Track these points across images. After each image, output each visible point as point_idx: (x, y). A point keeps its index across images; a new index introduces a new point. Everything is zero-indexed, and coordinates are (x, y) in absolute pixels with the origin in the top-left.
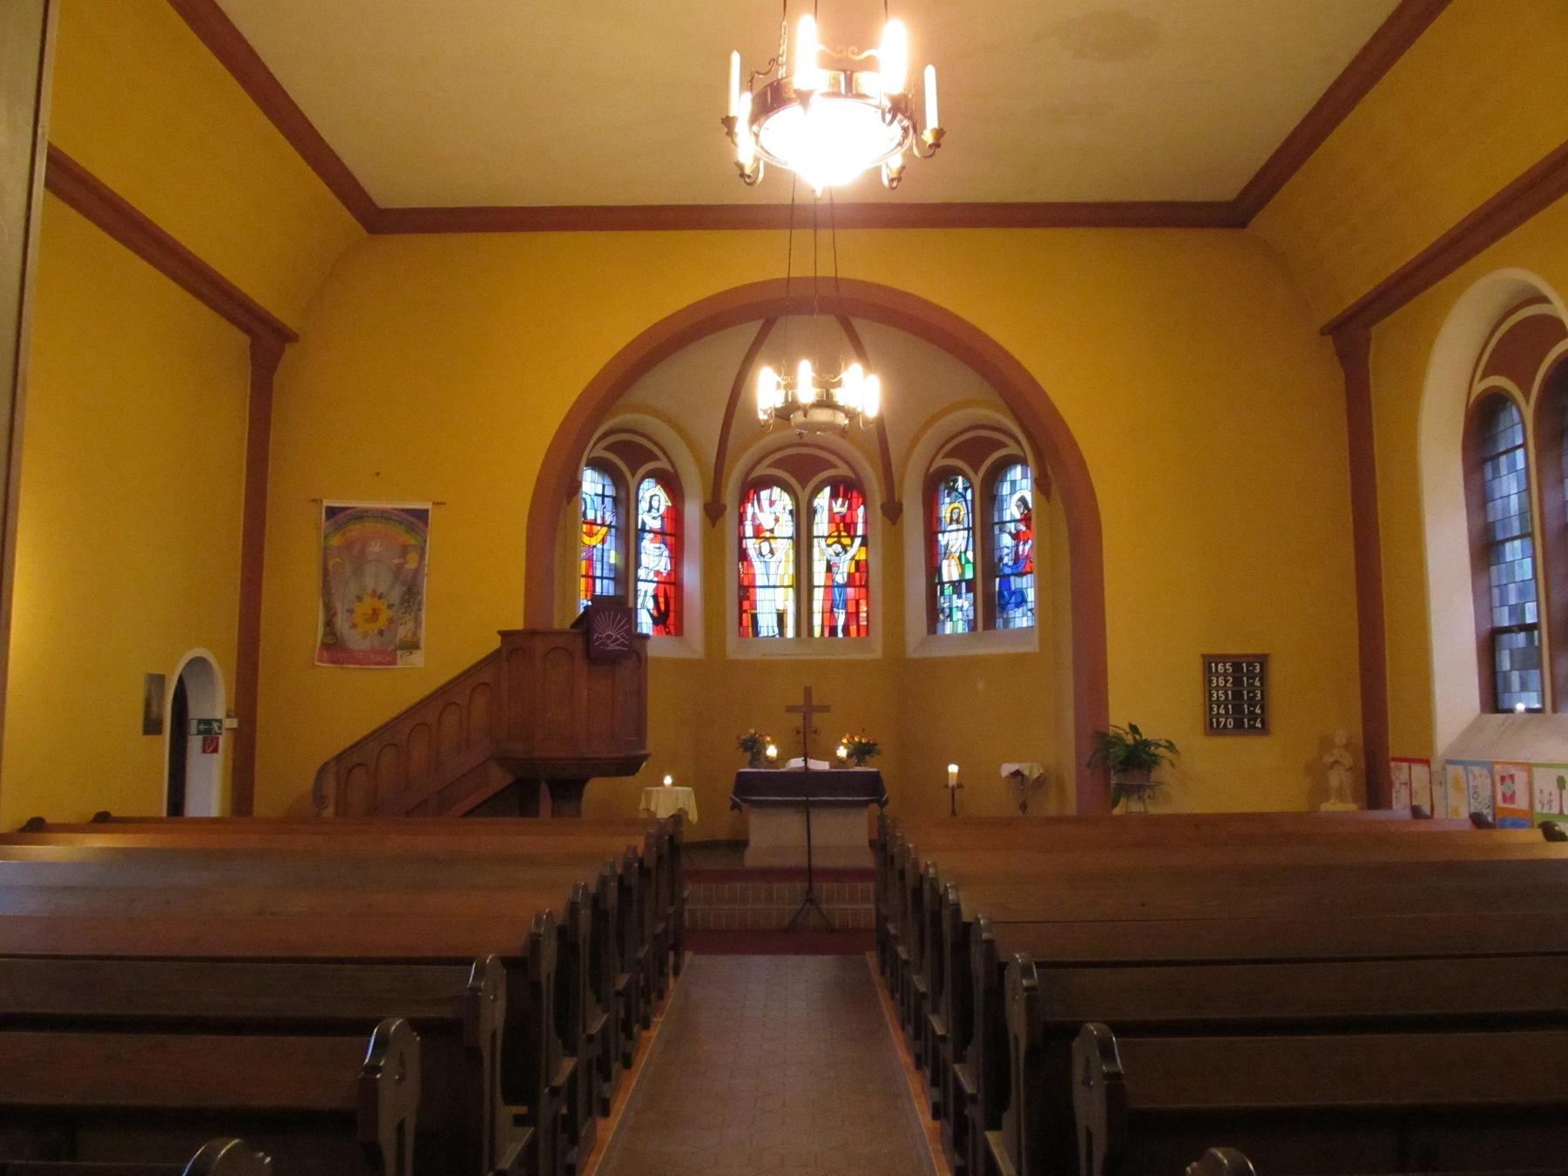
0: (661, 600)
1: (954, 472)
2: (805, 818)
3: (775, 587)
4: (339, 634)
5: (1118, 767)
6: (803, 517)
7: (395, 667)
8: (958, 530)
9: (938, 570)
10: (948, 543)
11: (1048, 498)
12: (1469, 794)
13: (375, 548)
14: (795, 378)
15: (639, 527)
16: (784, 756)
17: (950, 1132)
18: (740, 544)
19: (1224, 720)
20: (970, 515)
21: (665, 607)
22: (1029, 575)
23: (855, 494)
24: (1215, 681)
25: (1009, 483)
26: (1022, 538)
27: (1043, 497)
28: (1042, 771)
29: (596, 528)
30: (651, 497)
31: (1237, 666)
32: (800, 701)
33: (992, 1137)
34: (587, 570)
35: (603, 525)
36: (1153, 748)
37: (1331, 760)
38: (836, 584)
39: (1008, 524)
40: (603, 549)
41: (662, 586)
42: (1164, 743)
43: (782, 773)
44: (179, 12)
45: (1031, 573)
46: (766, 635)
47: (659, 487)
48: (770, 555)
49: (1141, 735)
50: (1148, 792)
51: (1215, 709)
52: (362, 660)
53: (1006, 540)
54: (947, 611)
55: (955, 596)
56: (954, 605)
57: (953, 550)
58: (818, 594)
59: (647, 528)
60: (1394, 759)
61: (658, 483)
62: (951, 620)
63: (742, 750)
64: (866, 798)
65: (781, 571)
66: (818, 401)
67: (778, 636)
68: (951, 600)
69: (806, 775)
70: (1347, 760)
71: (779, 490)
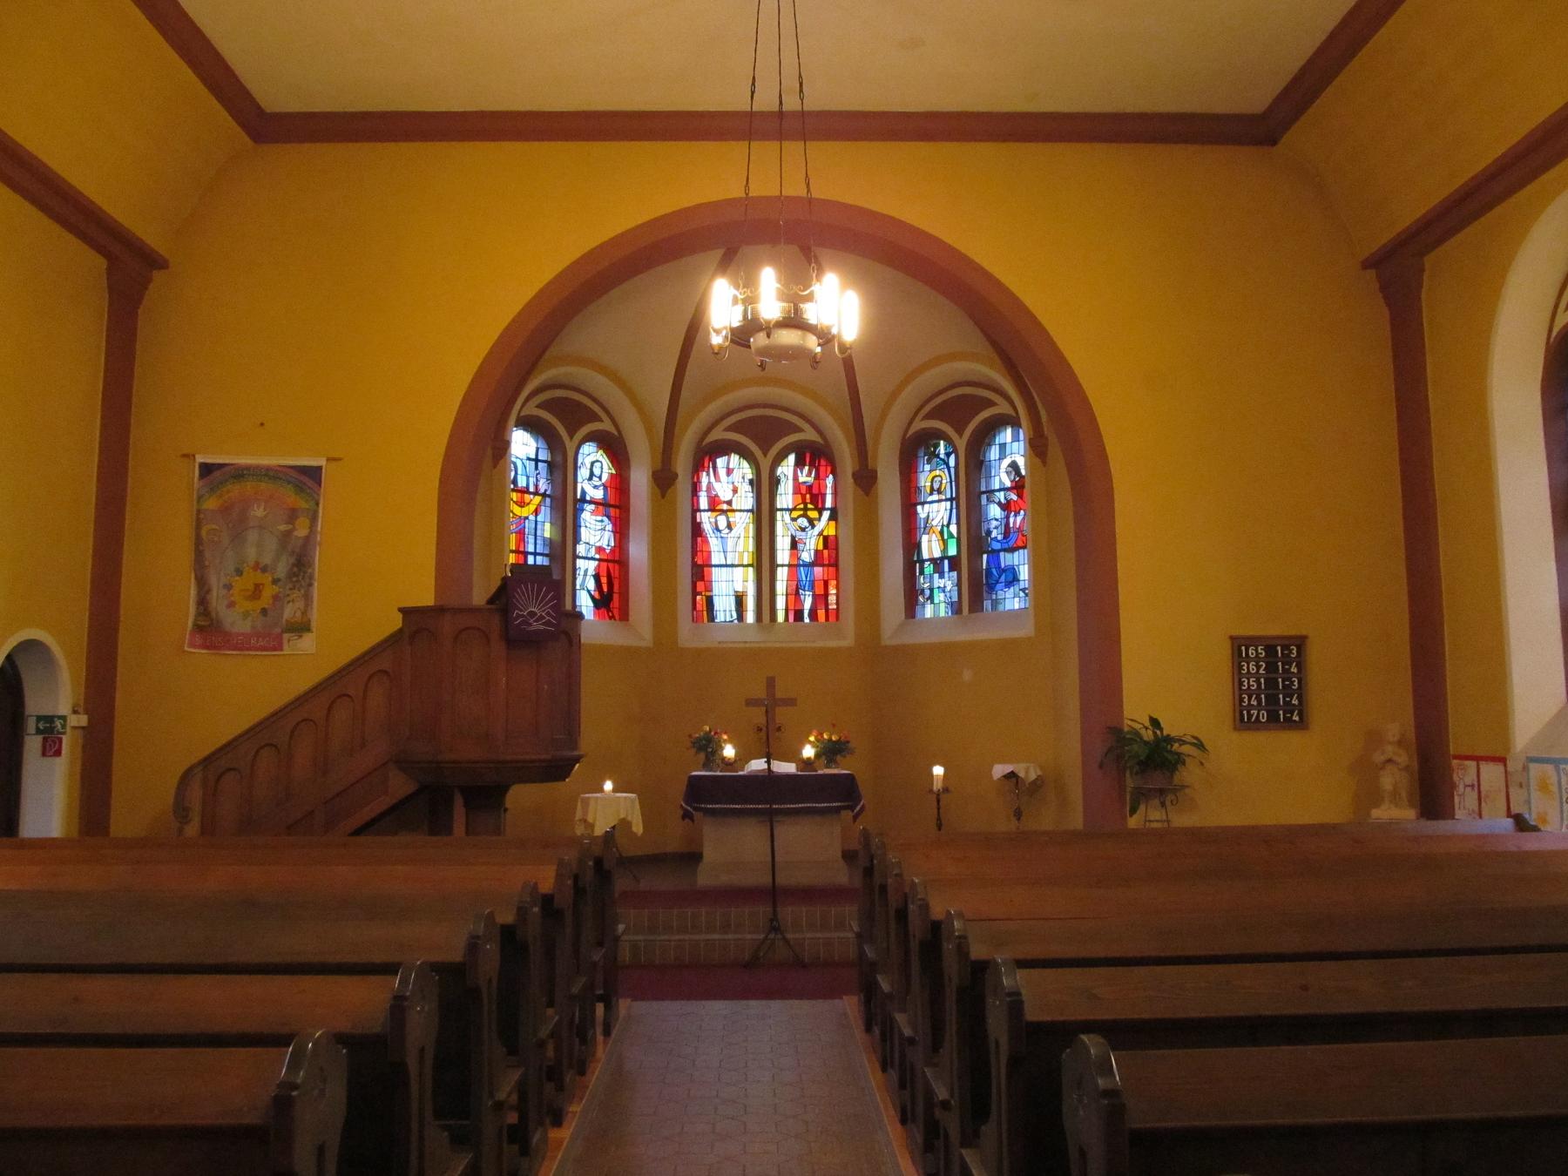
0: (604, 580)
1: (939, 435)
2: (769, 828)
3: (732, 566)
4: (214, 615)
5: (1137, 768)
6: (765, 487)
7: (282, 653)
8: (939, 501)
9: (918, 546)
10: (928, 516)
11: (1044, 463)
12: (1561, 798)
13: (258, 512)
14: (756, 289)
15: (579, 497)
16: (743, 758)
17: (919, 1139)
18: (694, 518)
19: (1256, 712)
20: (953, 483)
22: (1022, 551)
23: (823, 462)
24: (1245, 668)
25: (997, 447)
26: (1013, 509)
27: (1037, 460)
28: (1039, 773)
29: (527, 497)
31: (1270, 649)
33: (969, 1156)
34: (518, 545)
35: (536, 493)
36: (1176, 745)
37: (1383, 758)
39: (997, 494)
40: (536, 521)
42: (1188, 739)
43: (740, 776)
44: (159, 32)
45: (1024, 547)
46: (723, 620)
47: (601, 452)
48: (727, 531)
49: (1161, 730)
50: (1170, 797)
51: (1246, 700)
52: (241, 644)
53: (995, 511)
54: (927, 592)
55: (936, 576)
56: (936, 585)
57: (934, 523)
58: (782, 574)
59: (588, 498)
60: (1456, 757)
62: (932, 602)
63: (694, 750)
64: (839, 804)
65: (740, 548)
66: (784, 318)
67: (736, 621)
69: (769, 778)
70: (1403, 758)
71: (737, 457)
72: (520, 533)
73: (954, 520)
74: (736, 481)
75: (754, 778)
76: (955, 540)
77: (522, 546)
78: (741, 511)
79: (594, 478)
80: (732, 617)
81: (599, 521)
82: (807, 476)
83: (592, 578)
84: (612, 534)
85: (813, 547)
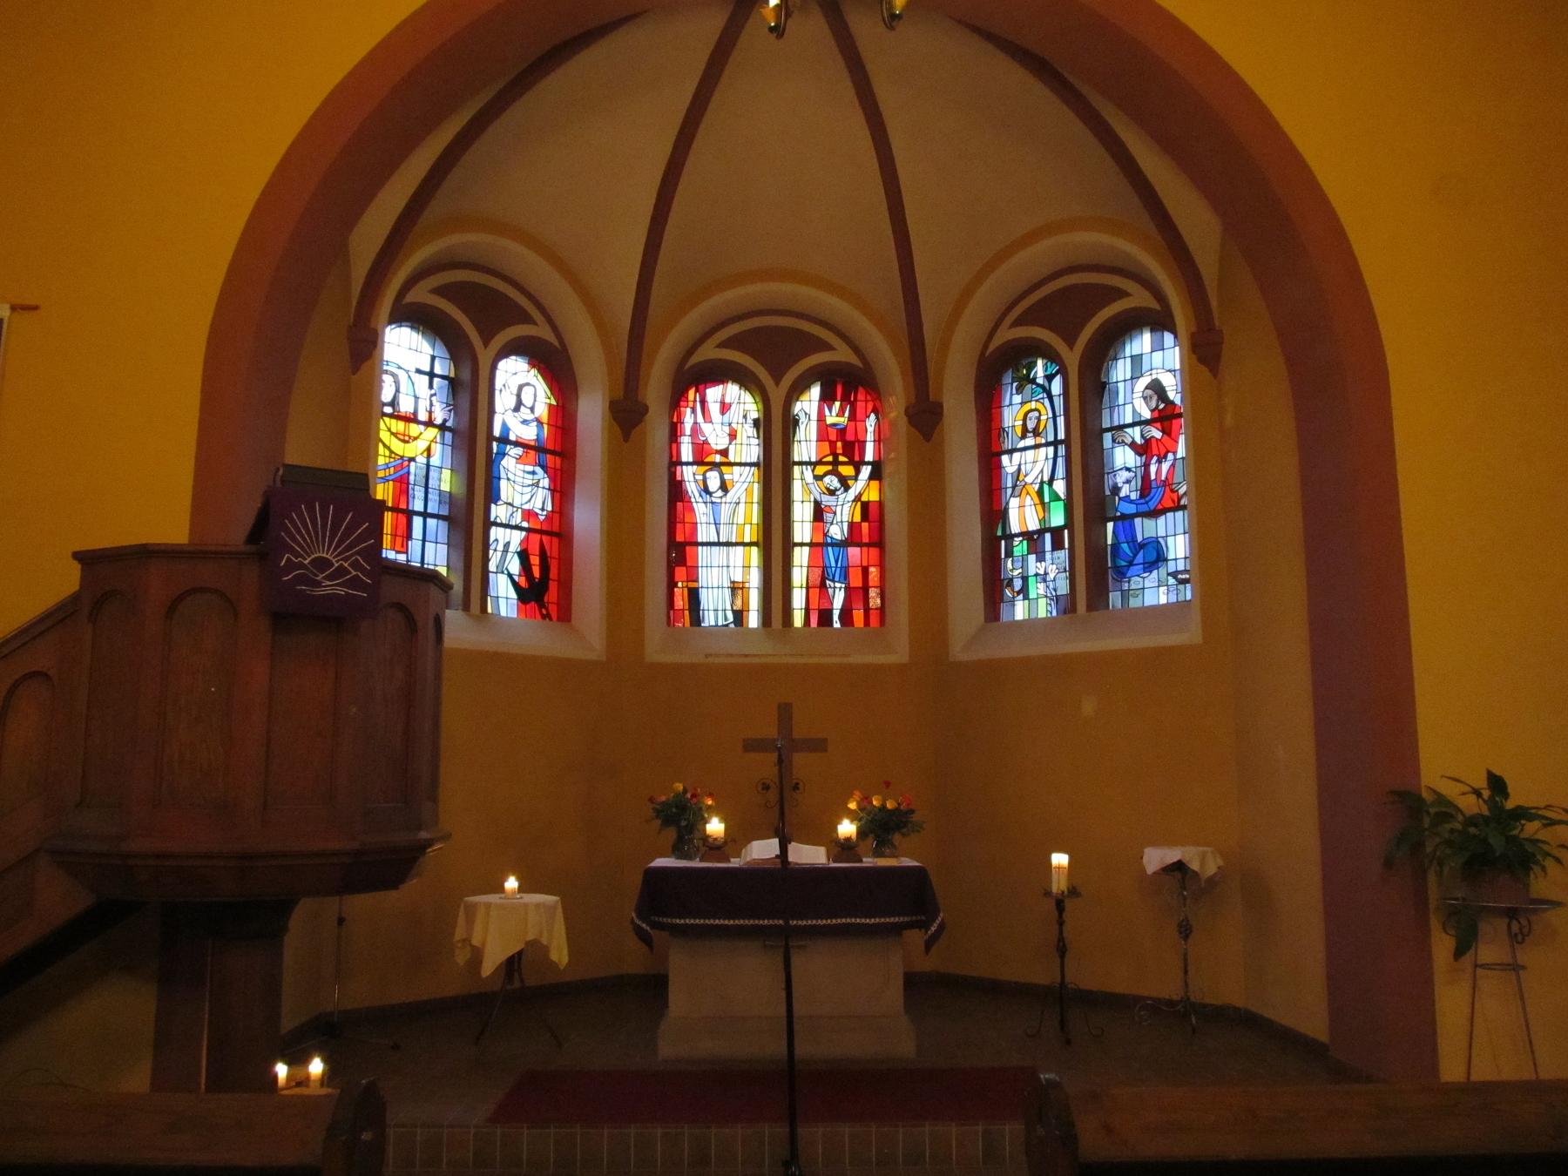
0: (535, 560)
2: (780, 958)
3: (728, 544)
8: (1037, 447)
9: (1003, 515)
10: (1019, 470)
16: (737, 838)
18: (672, 475)
21: (541, 572)
22: (1170, 515)
23: (860, 396)
25: (1128, 360)
26: (1155, 450)
28: (1220, 862)
29: (414, 429)
30: (521, 387)
32: (770, 731)
34: (396, 499)
35: (429, 423)
38: (829, 540)
39: (1129, 430)
40: (428, 466)
41: (536, 538)
46: (713, 623)
47: (534, 372)
48: (720, 493)
54: (1018, 584)
55: (1032, 558)
56: (1032, 571)
57: (1029, 479)
58: (801, 557)
61: (532, 364)
62: (1026, 597)
63: (659, 822)
67: (732, 626)
68: (1024, 566)
69: (782, 873)
72: (401, 482)
73: (1060, 472)
74: (735, 421)
75: (756, 875)
76: (1061, 503)
77: (403, 499)
78: (740, 464)
79: (522, 407)
80: (726, 619)
81: (529, 473)
82: (837, 416)
83: (516, 556)
84: (548, 494)
85: (845, 518)
